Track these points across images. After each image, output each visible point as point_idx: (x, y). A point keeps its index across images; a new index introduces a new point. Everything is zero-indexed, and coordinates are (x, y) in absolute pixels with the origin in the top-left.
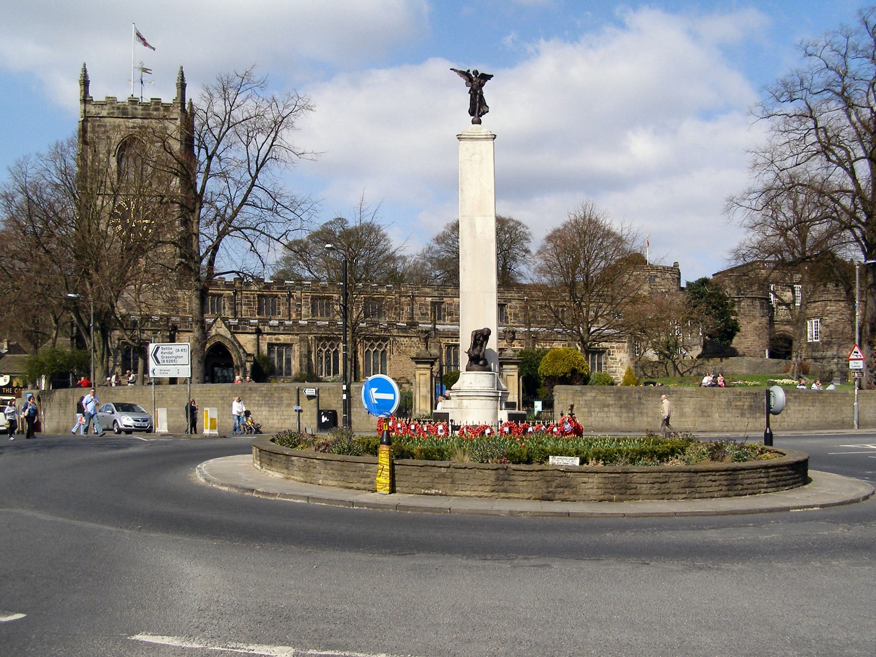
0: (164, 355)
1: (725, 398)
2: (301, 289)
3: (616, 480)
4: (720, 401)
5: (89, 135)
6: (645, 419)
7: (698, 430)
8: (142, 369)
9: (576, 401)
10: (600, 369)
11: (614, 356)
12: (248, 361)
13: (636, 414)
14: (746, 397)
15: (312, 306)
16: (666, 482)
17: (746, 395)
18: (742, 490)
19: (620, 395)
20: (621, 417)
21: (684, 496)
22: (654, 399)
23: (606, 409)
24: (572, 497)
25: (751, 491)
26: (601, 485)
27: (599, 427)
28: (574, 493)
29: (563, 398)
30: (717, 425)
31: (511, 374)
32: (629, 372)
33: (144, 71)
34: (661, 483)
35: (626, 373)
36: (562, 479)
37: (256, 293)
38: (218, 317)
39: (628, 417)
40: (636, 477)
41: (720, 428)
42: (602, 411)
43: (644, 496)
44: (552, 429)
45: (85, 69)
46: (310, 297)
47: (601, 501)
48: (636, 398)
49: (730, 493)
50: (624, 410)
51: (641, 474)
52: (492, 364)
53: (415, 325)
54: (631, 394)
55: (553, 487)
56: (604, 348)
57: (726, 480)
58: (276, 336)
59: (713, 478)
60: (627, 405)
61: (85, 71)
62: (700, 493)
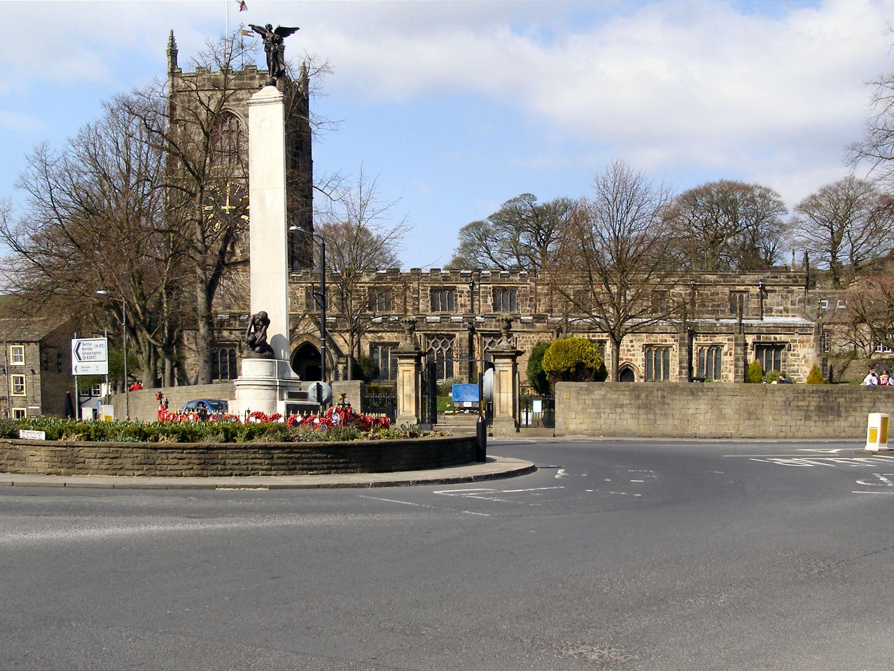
0: (85, 351)
1: (781, 397)
2: (419, 280)
3: (63, 454)
4: (773, 400)
5: (179, 111)
6: (670, 422)
7: (742, 436)
8: (169, 371)
9: (581, 401)
10: (777, 368)
11: (795, 352)
12: (339, 363)
13: (658, 416)
14: (812, 395)
15: (432, 299)
16: (117, 458)
17: (812, 393)
18: (221, 470)
19: (637, 393)
20: (638, 419)
21: (140, 472)
22: (682, 397)
23: (619, 410)
24: (22, 469)
25: (238, 472)
26: (48, 458)
27: (610, 431)
28: (23, 466)
29: (565, 396)
30: (771, 430)
31: (505, 369)
32: (814, 371)
33: (245, 35)
34: (111, 458)
35: (811, 373)
36: (12, 451)
37: (366, 285)
38: (306, 314)
39: (648, 419)
40: (83, 451)
41: (774, 434)
42: (614, 412)
43: (93, 471)
44: (313, 420)
45: (172, 37)
46: (429, 288)
47: (49, 474)
48: (658, 396)
49: (205, 472)
50: (642, 411)
51: (88, 448)
52: (282, 351)
53: (543, 318)
54: (652, 392)
55: (5, 459)
56: (783, 342)
57: (199, 459)
58: (380, 334)
59: (179, 456)
60: (646, 405)
61: (172, 39)
62: (161, 470)
